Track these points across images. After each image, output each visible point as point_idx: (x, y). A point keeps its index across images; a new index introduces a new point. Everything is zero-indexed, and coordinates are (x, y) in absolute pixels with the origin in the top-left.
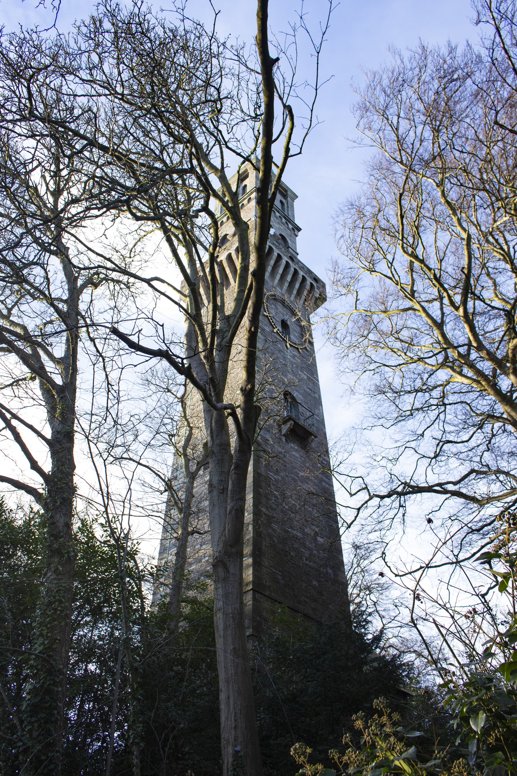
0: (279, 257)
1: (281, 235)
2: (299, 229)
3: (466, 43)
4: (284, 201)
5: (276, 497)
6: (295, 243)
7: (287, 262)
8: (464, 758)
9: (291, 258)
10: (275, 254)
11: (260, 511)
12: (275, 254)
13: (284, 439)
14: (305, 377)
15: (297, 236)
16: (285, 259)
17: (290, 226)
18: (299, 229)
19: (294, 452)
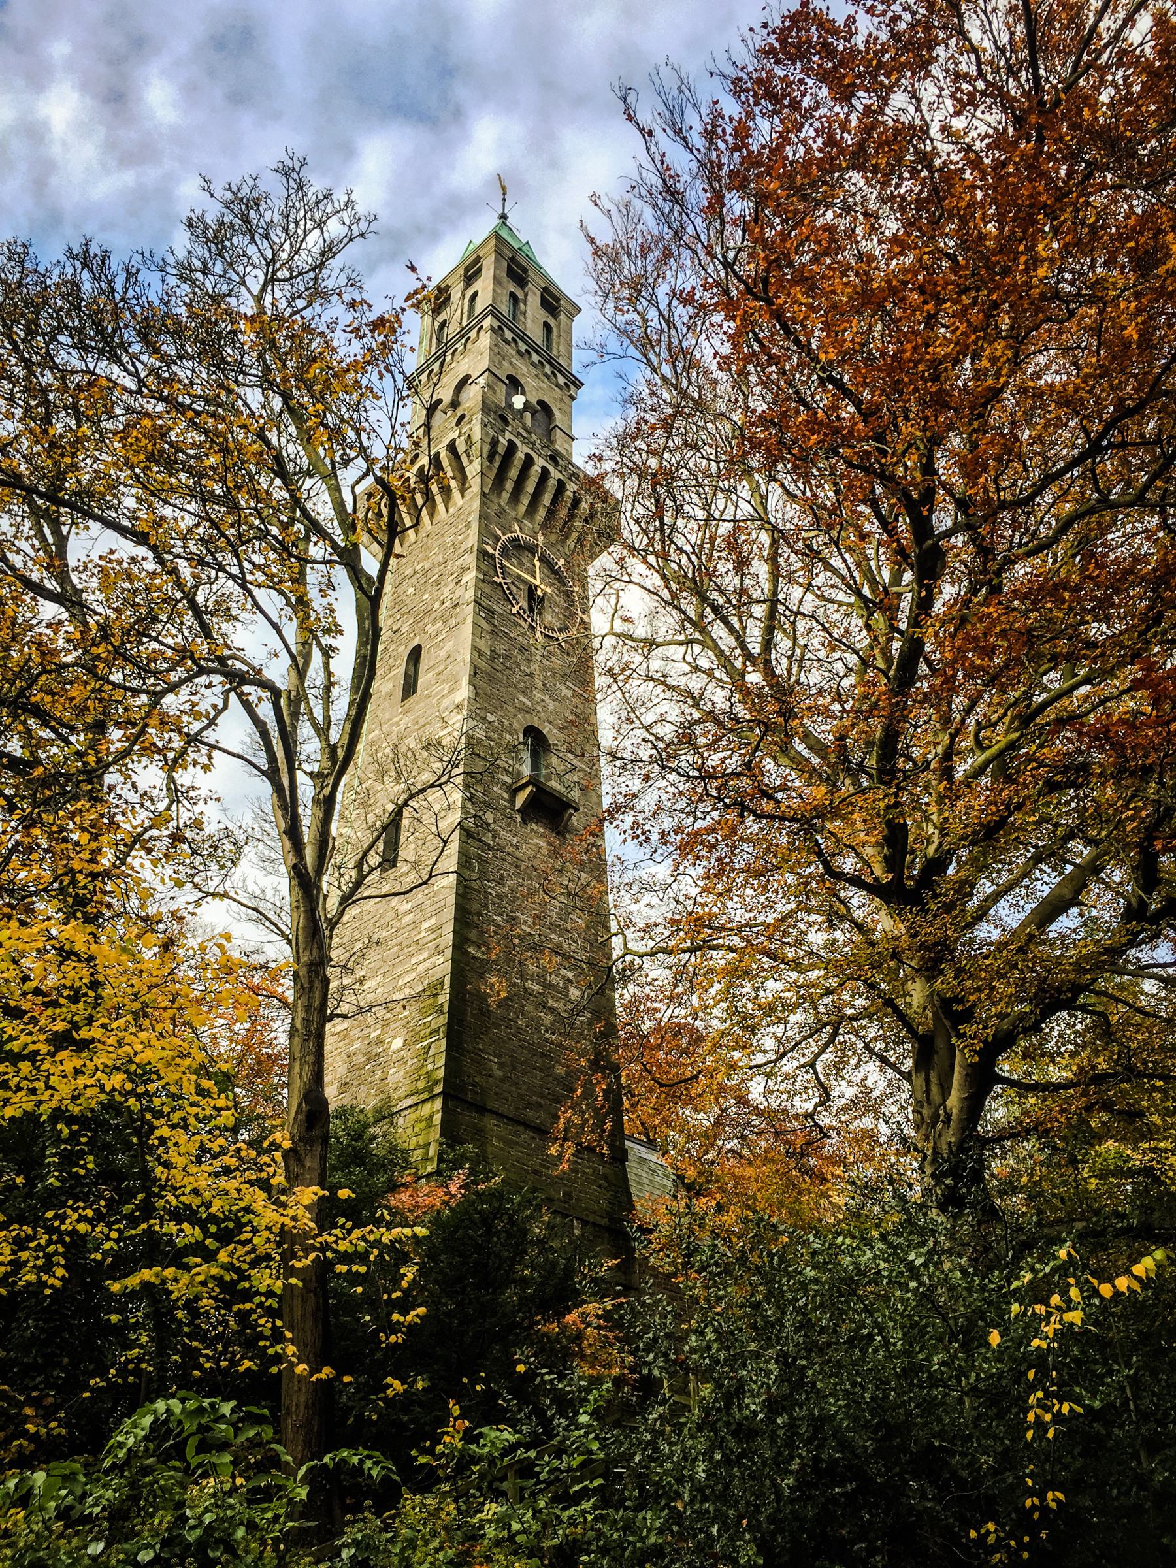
0: (529, 461)
1: (540, 402)
2: (578, 384)
3: (589, 248)
4: (552, 321)
5: (497, 925)
6: (569, 415)
7: (544, 469)
8: (1070, 1005)
9: (554, 458)
10: (520, 455)
11: (467, 953)
12: (520, 455)
13: (519, 818)
14: (569, 693)
15: (573, 398)
16: (540, 462)
17: (561, 380)
18: (578, 384)
19: (535, 841)
